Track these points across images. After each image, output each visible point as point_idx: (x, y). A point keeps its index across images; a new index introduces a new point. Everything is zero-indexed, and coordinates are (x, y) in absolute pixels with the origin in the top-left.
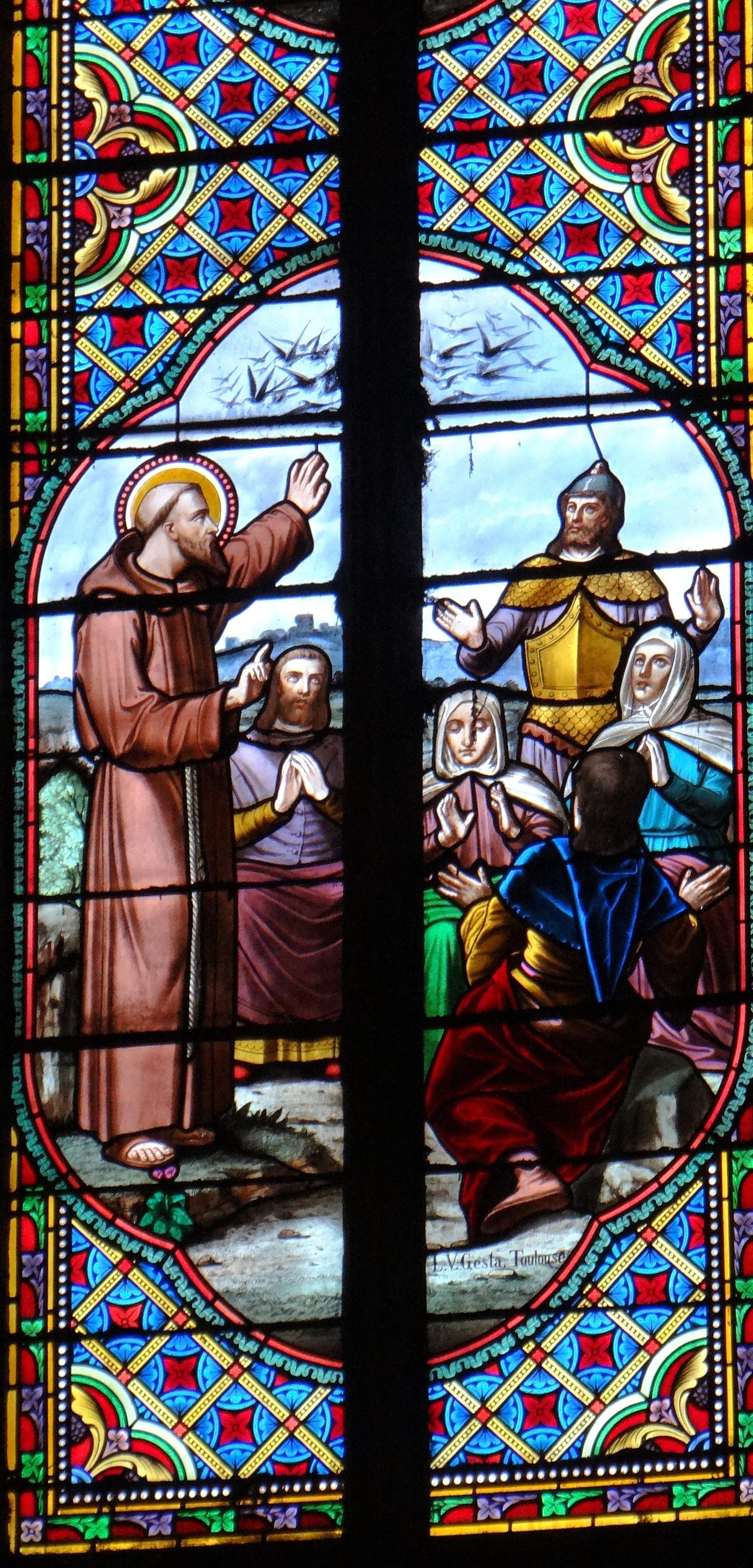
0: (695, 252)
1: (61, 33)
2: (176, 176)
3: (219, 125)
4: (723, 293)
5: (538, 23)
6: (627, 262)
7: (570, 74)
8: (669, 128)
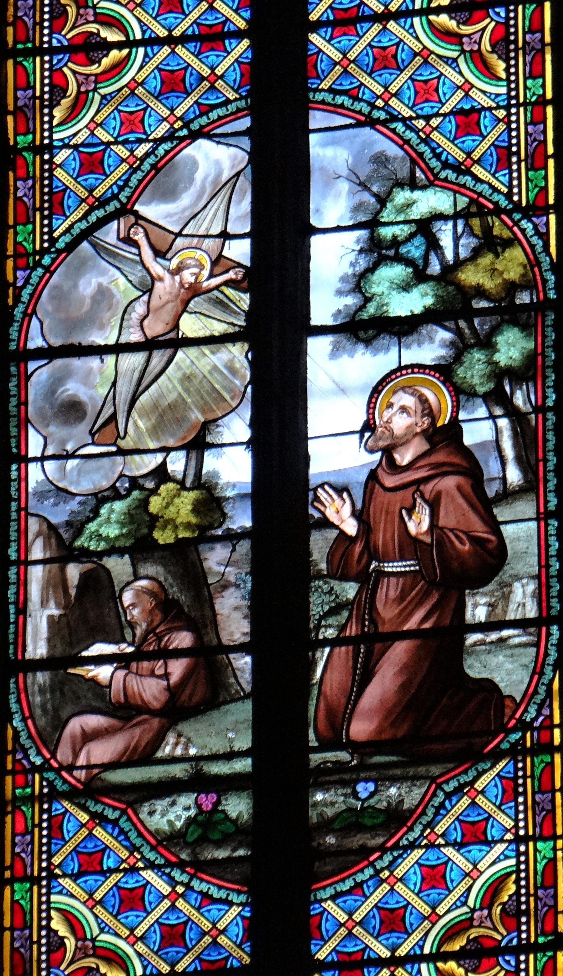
0: (510, 98)
1: (40, 887)
2: (129, 54)
3: (160, 957)
4: (538, 793)
5: (401, 880)
6: (459, 106)
7: (425, 918)
8: (500, 959)
